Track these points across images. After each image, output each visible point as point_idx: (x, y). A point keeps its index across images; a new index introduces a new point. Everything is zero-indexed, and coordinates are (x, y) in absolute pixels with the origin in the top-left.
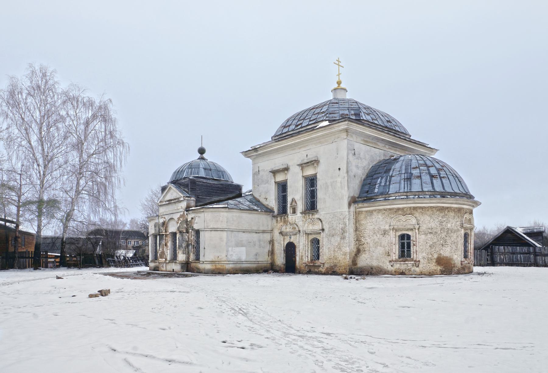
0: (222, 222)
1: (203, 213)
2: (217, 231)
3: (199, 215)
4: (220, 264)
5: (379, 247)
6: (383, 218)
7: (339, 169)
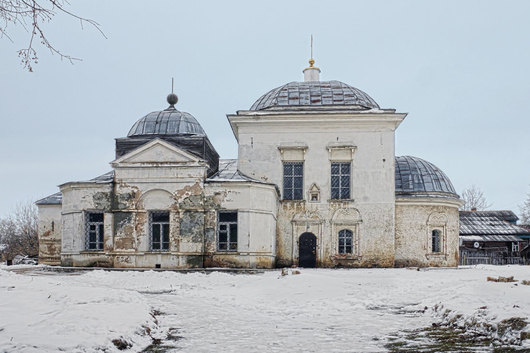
0: (267, 202)
1: (249, 188)
2: (262, 213)
3: (237, 190)
4: (264, 257)
5: (415, 241)
6: (420, 214)
7: (384, 160)
